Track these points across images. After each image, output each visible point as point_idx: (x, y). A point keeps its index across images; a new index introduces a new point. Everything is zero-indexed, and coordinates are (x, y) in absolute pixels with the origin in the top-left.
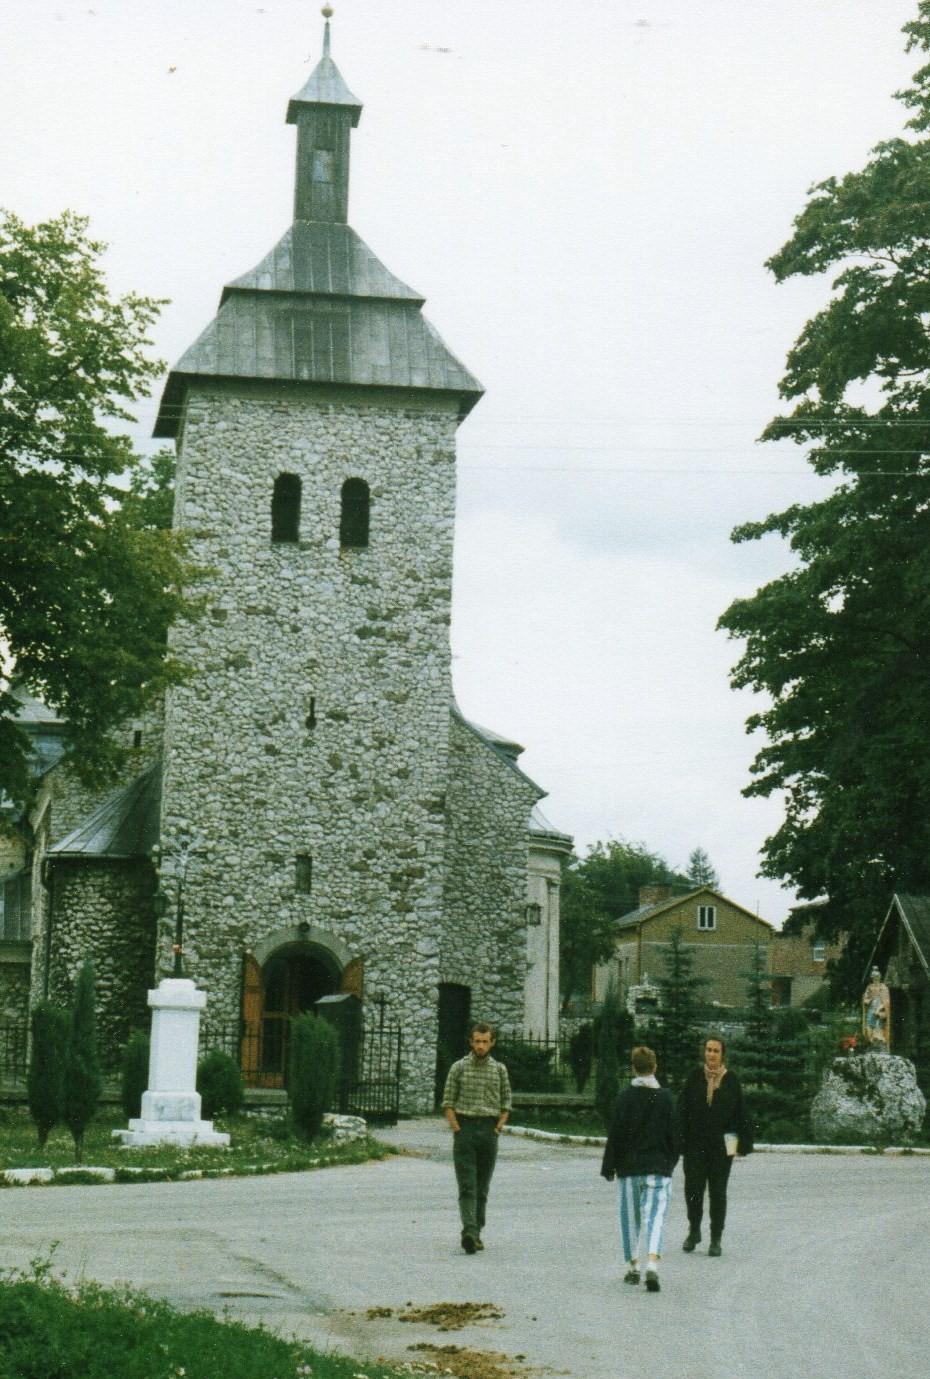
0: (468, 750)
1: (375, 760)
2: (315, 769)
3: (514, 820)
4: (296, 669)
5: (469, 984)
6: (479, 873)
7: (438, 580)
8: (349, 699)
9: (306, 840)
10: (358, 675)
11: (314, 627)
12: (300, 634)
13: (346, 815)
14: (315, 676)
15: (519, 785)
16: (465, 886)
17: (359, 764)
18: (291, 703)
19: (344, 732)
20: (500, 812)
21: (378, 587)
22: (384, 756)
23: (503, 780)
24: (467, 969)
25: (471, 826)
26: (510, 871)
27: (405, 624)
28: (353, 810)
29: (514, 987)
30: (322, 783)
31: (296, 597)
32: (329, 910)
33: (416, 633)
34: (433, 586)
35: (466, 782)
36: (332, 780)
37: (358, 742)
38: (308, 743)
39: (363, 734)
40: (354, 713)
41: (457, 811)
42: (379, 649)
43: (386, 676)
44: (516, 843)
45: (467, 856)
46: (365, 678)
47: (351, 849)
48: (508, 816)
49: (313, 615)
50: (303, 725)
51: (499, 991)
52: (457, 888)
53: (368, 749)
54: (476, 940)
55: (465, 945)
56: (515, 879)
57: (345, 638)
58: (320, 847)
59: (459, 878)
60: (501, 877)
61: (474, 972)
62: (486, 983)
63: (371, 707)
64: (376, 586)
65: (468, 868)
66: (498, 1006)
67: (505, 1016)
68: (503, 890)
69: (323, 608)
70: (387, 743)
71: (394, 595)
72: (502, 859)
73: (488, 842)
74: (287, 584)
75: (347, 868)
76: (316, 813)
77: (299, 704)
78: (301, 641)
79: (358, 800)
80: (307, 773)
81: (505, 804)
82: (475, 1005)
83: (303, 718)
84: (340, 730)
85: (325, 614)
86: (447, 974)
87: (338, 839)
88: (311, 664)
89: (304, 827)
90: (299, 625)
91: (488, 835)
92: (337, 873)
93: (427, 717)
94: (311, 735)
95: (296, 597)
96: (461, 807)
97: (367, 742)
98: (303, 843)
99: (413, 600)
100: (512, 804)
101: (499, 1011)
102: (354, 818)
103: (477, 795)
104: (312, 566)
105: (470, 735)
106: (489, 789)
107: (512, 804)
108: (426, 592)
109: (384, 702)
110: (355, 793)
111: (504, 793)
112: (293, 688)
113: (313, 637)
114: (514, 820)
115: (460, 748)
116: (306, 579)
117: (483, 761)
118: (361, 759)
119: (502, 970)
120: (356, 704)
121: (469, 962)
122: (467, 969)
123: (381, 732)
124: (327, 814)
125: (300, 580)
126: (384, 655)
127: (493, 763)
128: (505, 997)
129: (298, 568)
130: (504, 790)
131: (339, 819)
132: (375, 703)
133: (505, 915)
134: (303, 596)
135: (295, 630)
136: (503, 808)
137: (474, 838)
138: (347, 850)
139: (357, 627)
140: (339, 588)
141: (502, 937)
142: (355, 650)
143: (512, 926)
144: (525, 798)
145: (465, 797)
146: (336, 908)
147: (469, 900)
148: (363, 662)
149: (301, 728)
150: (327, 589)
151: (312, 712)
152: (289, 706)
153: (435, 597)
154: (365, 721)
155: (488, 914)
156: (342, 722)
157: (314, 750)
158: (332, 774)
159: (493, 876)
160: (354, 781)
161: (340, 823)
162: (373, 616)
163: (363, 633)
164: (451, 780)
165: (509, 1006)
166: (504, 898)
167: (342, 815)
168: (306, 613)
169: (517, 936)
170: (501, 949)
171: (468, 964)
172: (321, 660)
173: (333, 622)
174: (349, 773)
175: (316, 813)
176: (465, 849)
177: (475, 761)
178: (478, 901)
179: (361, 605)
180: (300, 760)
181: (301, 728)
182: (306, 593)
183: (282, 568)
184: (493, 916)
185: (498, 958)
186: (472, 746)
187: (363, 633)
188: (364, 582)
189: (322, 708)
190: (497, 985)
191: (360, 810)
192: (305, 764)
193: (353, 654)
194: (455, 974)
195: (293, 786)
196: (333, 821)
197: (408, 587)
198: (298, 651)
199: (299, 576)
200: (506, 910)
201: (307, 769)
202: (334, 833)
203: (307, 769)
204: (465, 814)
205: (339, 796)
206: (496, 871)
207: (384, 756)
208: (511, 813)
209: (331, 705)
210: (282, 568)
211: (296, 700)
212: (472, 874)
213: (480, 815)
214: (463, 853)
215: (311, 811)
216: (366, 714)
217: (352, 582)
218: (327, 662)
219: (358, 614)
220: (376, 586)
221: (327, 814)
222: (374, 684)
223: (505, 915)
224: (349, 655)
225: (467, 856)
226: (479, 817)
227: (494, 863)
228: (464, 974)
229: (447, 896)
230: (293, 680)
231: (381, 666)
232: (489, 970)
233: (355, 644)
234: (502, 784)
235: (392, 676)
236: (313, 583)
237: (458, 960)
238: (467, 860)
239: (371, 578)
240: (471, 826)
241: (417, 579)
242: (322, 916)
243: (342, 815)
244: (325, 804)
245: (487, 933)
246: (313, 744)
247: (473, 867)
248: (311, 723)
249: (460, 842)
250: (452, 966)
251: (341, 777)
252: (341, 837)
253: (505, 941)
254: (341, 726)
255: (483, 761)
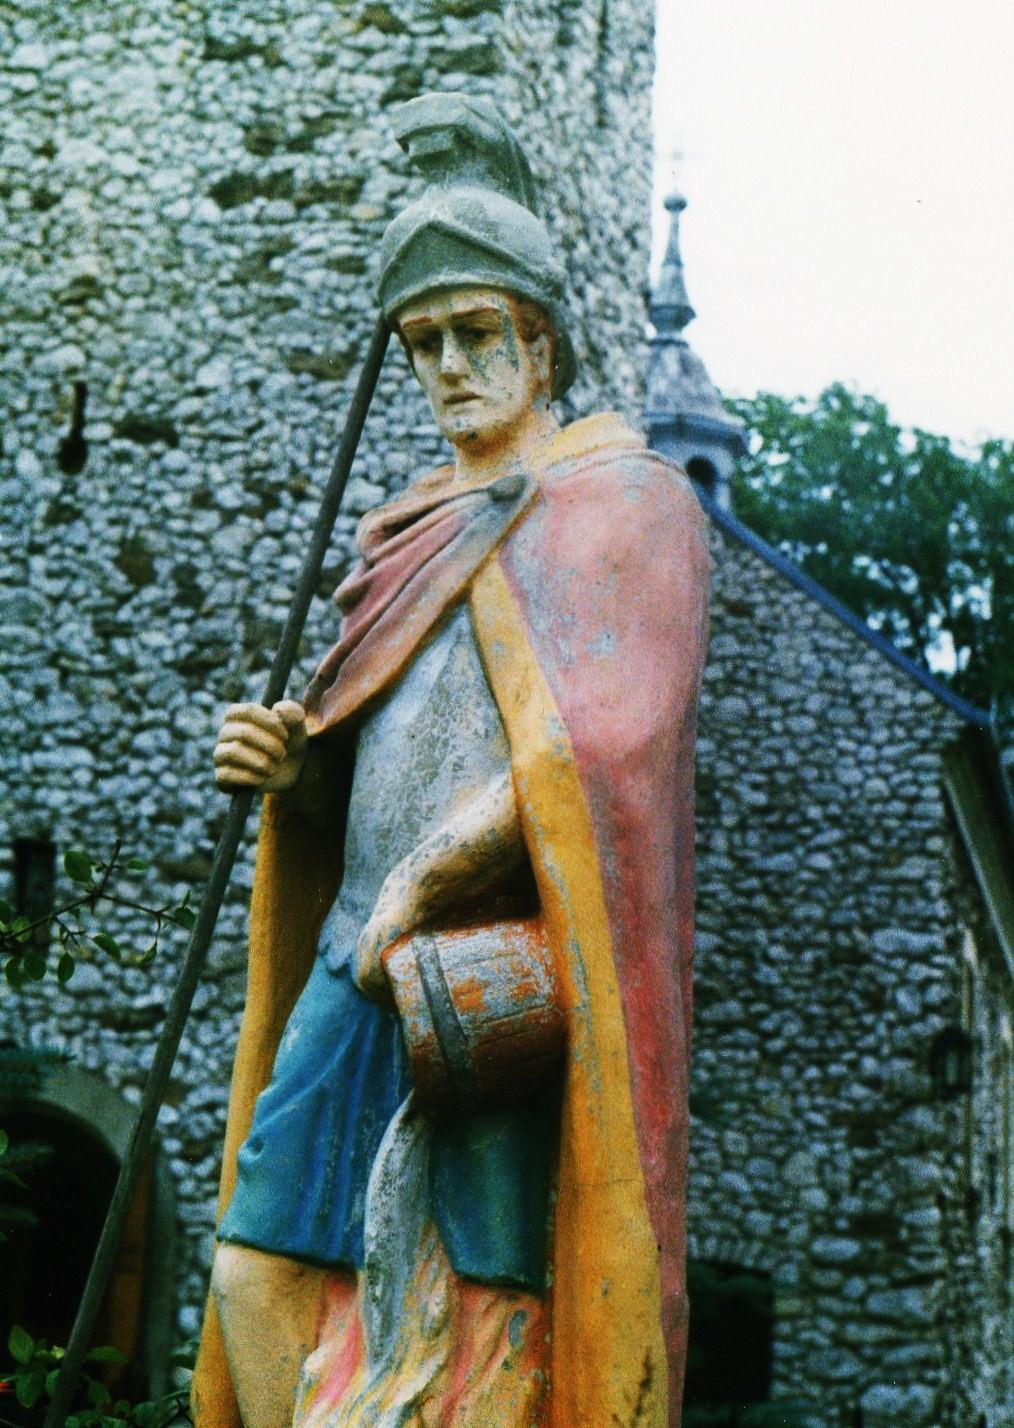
0: (761, 613)
1: (248, 550)
2: (79, 588)
3: (894, 795)
4: (38, 309)
5: (767, 1264)
6: (795, 948)
7: (451, 23)
8: (182, 378)
9: (41, 794)
10: (209, 310)
11: (96, 191)
12: (55, 211)
13: (162, 715)
14: (89, 324)
15: (904, 697)
16: (754, 984)
17: (204, 562)
18: (21, 403)
19: (164, 473)
20: (852, 776)
21: (280, 63)
22: (277, 535)
23: (856, 688)
24: (759, 1220)
25: (773, 818)
26: (885, 939)
27: (353, 154)
28: (181, 698)
29: (900, 1274)
30: (96, 625)
31: (52, 115)
32: (97, 1004)
33: (382, 171)
34: (439, 41)
35: (759, 700)
36: (124, 614)
37: (203, 499)
38: (62, 513)
39: (217, 473)
40: (193, 419)
41: (731, 779)
42: (272, 230)
43: (285, 304)
44: (899, 863)
45: (760, 901)
46: (230, 317)
47: (172, 816)
48: (877, 785)
49: (96, 156)
50: (53, 463)
51: (857, 1285)
52: (734, 991)
53: (229, 517)
54: (789, 1140)
55: (753, 1152)
56: (899, 963)
57: (180, 209)
58: (81, 814)
59: (737, 964)
60: (857, 957)
61: (783, 1232)
62: (821, 1263)
63: (245, 396)
64: (275, 62)
65: (761, 935)
66: (852, 1331)
67: (874, 1362)
68: (864, 995)
69: (124, 135)
70: (286, 497)
71: (323, 79)
72: (858, 906)
73: (822, 861)
74: (27, 82)
75: (153, 873)
76: (74, 712)
77: (40, 405)
78: (58, 233)
79: (194, 670)
80: (56, 600)
81: (867, 752)
82: (785, 1328)
83: (50, 444)
84: (154, 468)
85: (128, 151)
86: (702, 1239)
87: (131, 787)
88: (79, 291)
89: (39, 757)
90: (55, 187)
91: (821, 839)
92: (126, 890)
93: (410, 412)
94: (70, 488)
95: (52, 115)
96: (744, 769)
97: (228, 497)
98: (28, 805)
99: (380, 86)
100: (890, 751)
101: (856, 1347)
102: (182, 721)
103: (787, 732)
104: (97, 28)
105: (766, 573)
106: (820, 717)
107: (890, 751)
108: (419, 59)
109: (282, 380)
110: (186, 649)
111: (861, 723)
112: (28, 361)
113: (89, 218)
114: (894, 795)
115: (741, 609)
116: (82, 62)
117: (802, 640)
118: (208, 549)
119: (863, 1226)
120: (200, 392)
121: (766, 1202)
122: (759, 1220)
123: (269, 466)
124: (105, 713)
125: (61, 70)
126: (286, 246)
127: (831, 642)
128: (875, 1304)
129: (62, 36)
130: (862, 713)
131: (139, 728)
132: (255, 385)
133: (869, 1064)
134: (70, 110)
135: (43, 201)
136: (860, 764)
137: (779, 849)
138: (155, 820)
139: (215, 177)
140: (169, 74)
141: (863, 1128)
142: (205, 238)
143: (889, 1098)
144: (923, 733)
145: (756, 741)
146: (120, 998)
147: (768, 1025)
148: (225, 274)
149: (46, 473)
150: (138, 85)
151: (80, 422)
152: (15, 414)
153: (443, 71)
154: (226, 439)
155: (822, 1064)
156: (158, 446)
157: (78, 533)
158: (124, 599)
159: (837, 956)
160: (188, 613)
161: (144, 740)
162: (262, 143)
163: (228, 192)
164: (718, 697)
165: (887, 1332)
166: (868, 1019)
167: (148, 715)
168: (74, 154)
169: (910, 1127)
170: (857, 1162)
171: (765, 1208)
172: (108, 279)
173: (146, 170)
174: (172, 591)
175: (74, 712)
176: (754, 882)
177: (780, 640)
178: (793, 1028)
179: (229, 116)
180: (38, 563)
181: (46, 473)
182: (78, 98)
183: (17, 41)
184: (835, 1069)
185: (854, 1188)
186: (771, 603)
187: (228, 192)
188: (245, 49)
189: (105, 411)
190: (850, 1268)
191: (204, 697)
192: (51, 575)
193: (200, 252)
194: (723, 1237)
195: (16, 639)
196: (123, 734)
197: (368, 52)
198: (47, 260)
199: (62, 58)
200: (874, 1052)
201: (56, 587)
202: (123, 770)
203: (56, 587)
204: (756, 787)
205: (142, 660)
206: (843, 939)
207: (277, 535)
208: (886, 777)
209: (132, 400)
210: (17, 41)
211: (33, 395)
212: (776, 951)
213: (799, 785)
214: (750, 894)
215: (61, 707)
216: (228, 415)
217: (208, 57)
218: (124, 282)
219: (220, 143)
220: (275, 62)
221: (105, 713)
222: (254, 331)
223: (869, 1064)
224: (188, 257)
225: (760, 901)
226: (795, 793)
227: (839, 918)
228: (749, 1236)
229: (707, 1014)
230: (28, 341)
231: (277, 278)
232: (825, 1225)
233: (204, 225)
234: (855, 699)
235: (307, 303)
236: (101, 72)
237: (734, 1196)
238: (758, 913)
239: (260, 40)
240: (773, 818)
241: (394, 27)
242: (76, 1022)
243: (148, 715)
244: (103, 685)
245: (818, 1119)
246: (77, 515)
247: (779, 933)
248: (72, 455)
249: (742, 863)
250: (716, 1213)
251: (152, 604)
252: (144, 782)
253: (870, 1142)
254: (157, 456)
255: (802, 640)
